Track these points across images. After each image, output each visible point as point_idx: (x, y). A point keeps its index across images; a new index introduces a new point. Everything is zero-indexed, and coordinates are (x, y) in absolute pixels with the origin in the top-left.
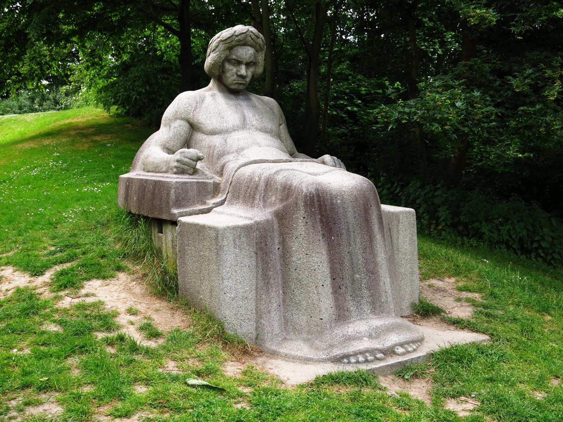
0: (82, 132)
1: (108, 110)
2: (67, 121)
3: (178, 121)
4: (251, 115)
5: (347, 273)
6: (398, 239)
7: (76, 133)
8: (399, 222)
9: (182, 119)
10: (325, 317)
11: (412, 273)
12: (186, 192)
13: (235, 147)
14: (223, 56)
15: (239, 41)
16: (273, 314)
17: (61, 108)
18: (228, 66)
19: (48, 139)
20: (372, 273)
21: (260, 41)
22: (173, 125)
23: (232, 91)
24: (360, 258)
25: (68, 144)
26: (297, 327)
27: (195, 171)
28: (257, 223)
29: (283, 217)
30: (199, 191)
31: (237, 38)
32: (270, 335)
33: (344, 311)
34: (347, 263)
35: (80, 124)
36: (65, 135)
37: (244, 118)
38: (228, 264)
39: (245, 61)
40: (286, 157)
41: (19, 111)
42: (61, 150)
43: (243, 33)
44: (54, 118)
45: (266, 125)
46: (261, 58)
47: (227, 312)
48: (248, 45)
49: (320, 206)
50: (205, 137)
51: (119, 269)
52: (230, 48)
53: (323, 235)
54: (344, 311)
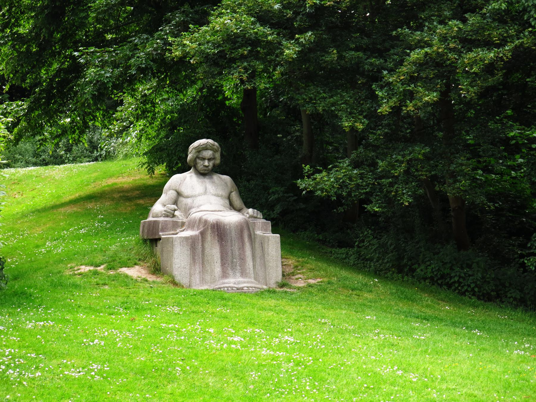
0: (126, 194)
1: (151, 170)
2: (111, 182)
5: (230, 258)
6: (268, 249)
7: (120, 197)
9: (173, 190)
10: (217, 275)
11: (277, 267)
12: (167, 225)
13: (197, 205)
14: (195, 156)
15: (203, 148)
16: (196, 275)
17: (101, 155)
18: (198, 161)
19: (91, 202)
20: (243, 259)
21: (215, 147)
22: (168, 193)
23: (203, 174)
25: (111, 207)
27: (174, 216)
28: (191, 236)
29: (203, 234)
35: (125, 186)
36: (109, 198)
38: (177, 252)
40: (222, 208)
41: (34, 160)
42: (105, 213)
44: (94, 175)
45: (218, 192)
46: (218, 155)
47: (176, 273)
49: (218, 229)
50: (184, 199)
51: (136, 264)
52: (199, 152)
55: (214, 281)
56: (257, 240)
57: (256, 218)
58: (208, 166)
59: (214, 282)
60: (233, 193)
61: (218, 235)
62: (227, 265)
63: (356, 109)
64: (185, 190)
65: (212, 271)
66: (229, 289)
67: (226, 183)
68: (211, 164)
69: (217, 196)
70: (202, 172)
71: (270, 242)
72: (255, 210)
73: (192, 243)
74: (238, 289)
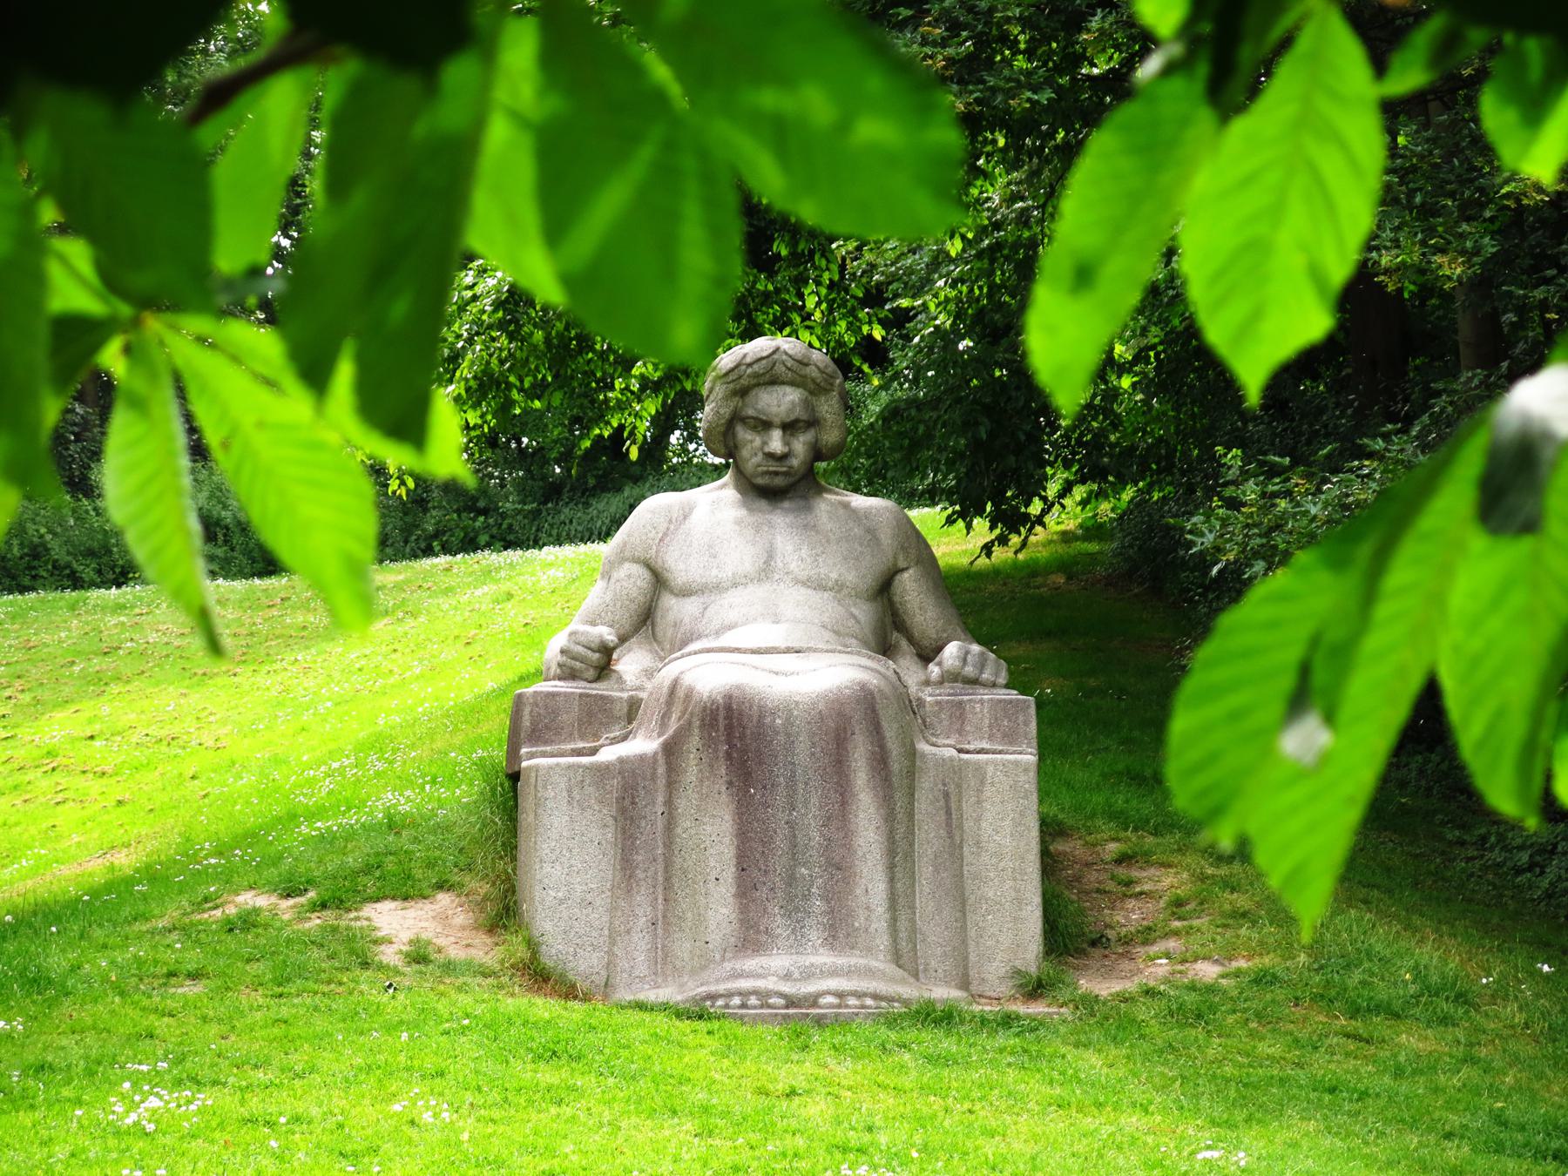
3: (627, 565)
4: (790, 548)
5: (779, 863)
6: (978, 820)
8: (982, 783)
9: (636, 560)
10: (715, 938)
11: (1019, 902)
12: (555, 713)
13: (716, 624)
14: (726, 411)
15: (756, 375)
18: (743, 434)
20: (839, 868)
21: (812, 372)
22: (615, 575)
23: (775, 489)
24: (814, 835)
26: (678, 964)
29: (671, 750)
30: (590, 714)
31: (749, 371)
32: (625, 975)
33: (758, 932)
34: (780, 842)
37: (770, 555)
38: (554, 834)
39: (777, 421)
40: (823, 638)
43: (762, 358)
47: (548, 926)
48: (783, 383)
49: (729, 728)
51: (441, 886)
52: (743, 392)
53: (730, 784)
54: (758, 932)
55: (704, 964)
56: (926, 787)
57: (974, 682)
58: (784, 457)
59: (704, 968)
60: (906, 575)
61: (728, 756)
62: (763, 893)
63: (1452, 195)
64: (682, 566)
65: (700, 919)
66: (753, 1001)
67: (871, 532)
68: (800, 445)
69: (819, 586)
70: (760, 481)
71: (988, 791)
72: (976, 648)
73: (628, 792)
74: (791, 1002)
